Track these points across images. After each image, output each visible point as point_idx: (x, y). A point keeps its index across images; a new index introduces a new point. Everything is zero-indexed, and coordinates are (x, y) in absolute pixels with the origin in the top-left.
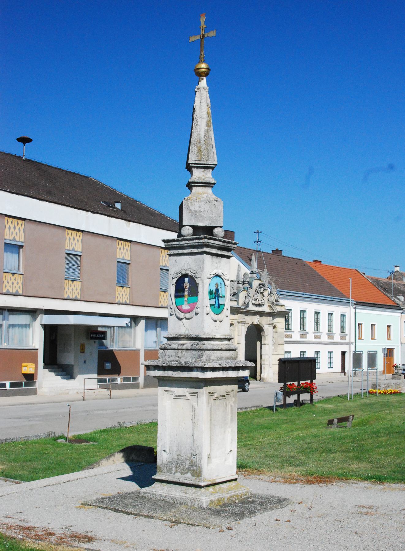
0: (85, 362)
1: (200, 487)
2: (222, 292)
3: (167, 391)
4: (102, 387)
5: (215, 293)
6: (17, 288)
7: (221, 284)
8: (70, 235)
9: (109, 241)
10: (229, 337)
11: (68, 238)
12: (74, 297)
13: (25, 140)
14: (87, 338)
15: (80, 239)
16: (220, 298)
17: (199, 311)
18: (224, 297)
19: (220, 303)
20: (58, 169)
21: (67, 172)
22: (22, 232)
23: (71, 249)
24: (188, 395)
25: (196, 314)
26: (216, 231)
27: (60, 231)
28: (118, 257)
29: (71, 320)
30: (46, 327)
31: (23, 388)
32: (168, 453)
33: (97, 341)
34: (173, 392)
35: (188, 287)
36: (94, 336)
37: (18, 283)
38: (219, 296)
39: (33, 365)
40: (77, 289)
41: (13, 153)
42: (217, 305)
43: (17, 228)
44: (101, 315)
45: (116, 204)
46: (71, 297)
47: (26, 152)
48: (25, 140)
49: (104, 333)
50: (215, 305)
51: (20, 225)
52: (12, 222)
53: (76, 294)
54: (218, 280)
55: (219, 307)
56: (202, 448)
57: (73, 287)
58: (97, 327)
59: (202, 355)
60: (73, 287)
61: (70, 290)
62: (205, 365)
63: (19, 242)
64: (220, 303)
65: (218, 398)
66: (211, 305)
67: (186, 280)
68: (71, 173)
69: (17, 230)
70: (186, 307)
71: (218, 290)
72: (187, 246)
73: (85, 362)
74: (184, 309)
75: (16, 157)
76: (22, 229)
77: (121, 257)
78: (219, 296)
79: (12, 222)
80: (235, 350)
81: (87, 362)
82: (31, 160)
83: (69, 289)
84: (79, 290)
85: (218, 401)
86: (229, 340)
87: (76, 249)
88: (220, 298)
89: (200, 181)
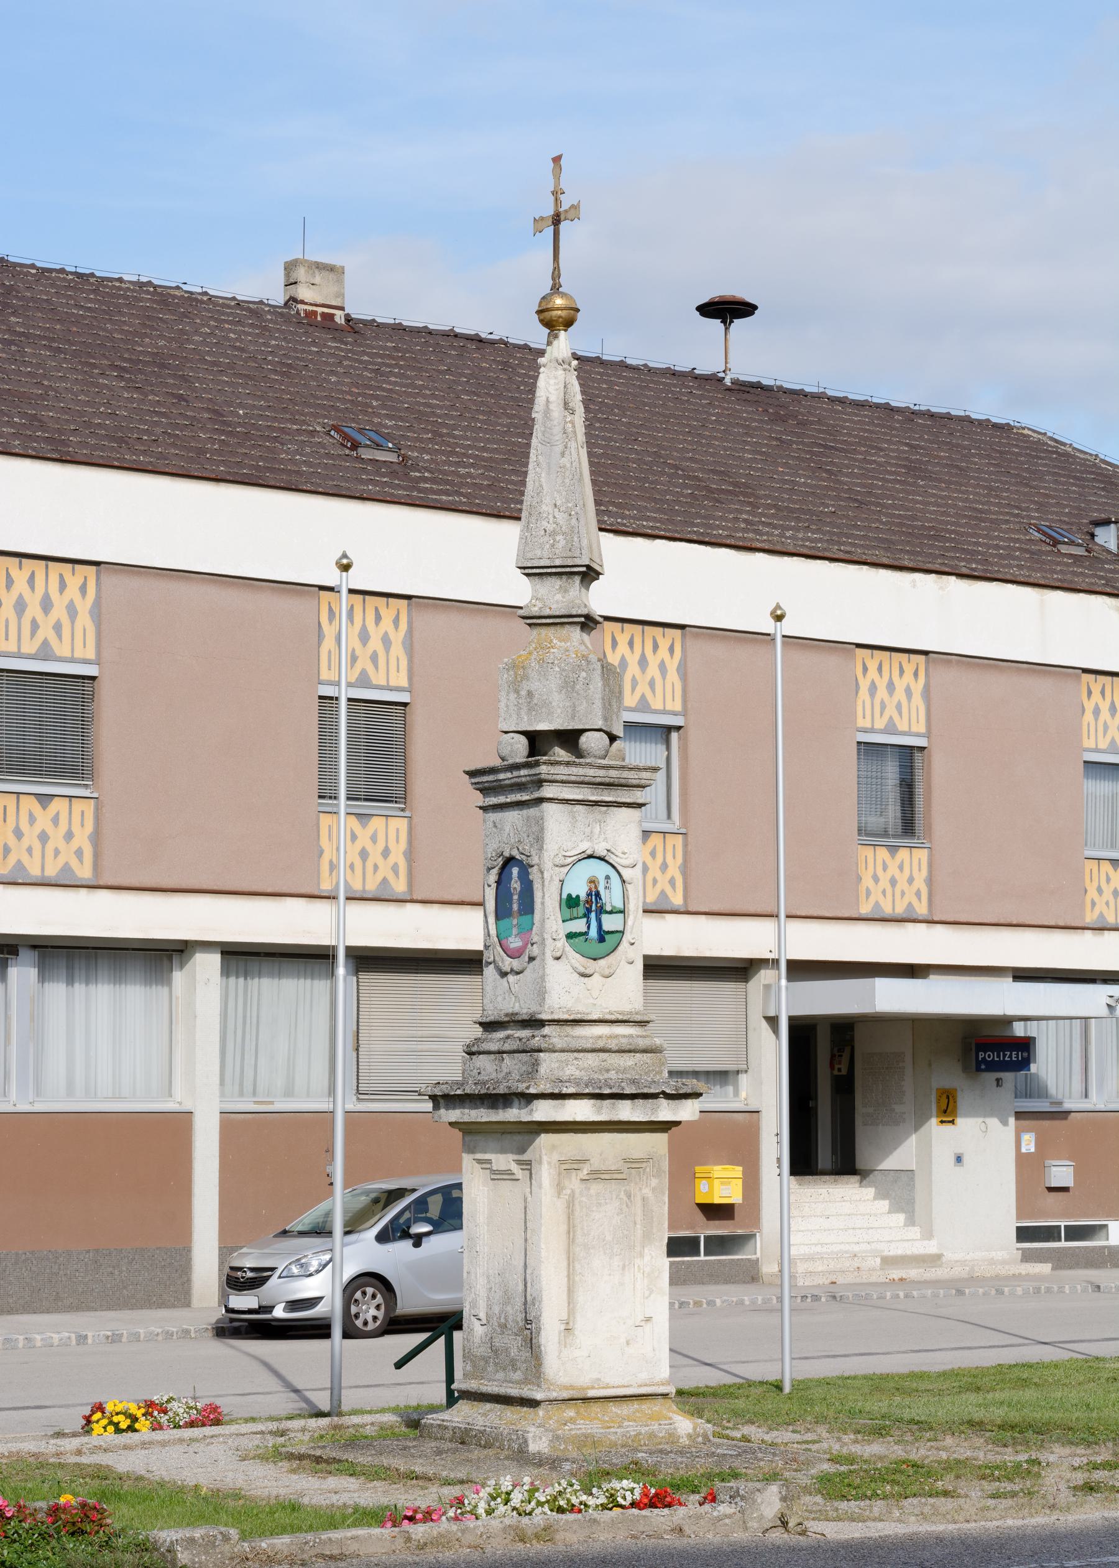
0: (959, 1159)
1: (533, 1403)
2: (612, 897)
3: (479, 1161)
4: (1028, 1257)
5: (588, 902)
6: (663, 884)
7: (608, 877)
8: (872, 672)
9: (1043, 686)
10: (638, 1018)
11: (864, 685)
12: (900, 910)
13: (726, 310)
14: (966, 1069)
15: (918, 687)
16: (604, 917)
17: (535, 950)
18: (622, 912)
19: (606, 927)
20: (878, 406)
21: (910, 415)
22: (673, 676)
23: (880, 724)
24: (515, 1168)
25: (532, 959)
26: (585, 740)
27: (832, 661)
28: (1089, 743)
29: (891, 997)
30: (803, 1035)
31: (702, 1258)
32: (484, 1322)
33: (1008, 1077)
34: (489, 1162)
35: (519, 889)
36: (991, 1056)
37: (664, 867)
38: (601, 910)
39: (738, 1171)
40: (911, 880)
41: (683, 366)
42: (593, 933)
43: (653, 661)
44: (1023, 975)
45: (1099, 531)
46: (888, 910)
47: (747, 354)
48: (726, 310)
49: (1026, 1045)
50: (586, 933)
51: (663, 652)
52: (631, 644)
53: (910, 897)
54: (599, 870)
55: (601, 939)
56: (540, 1302)
57: (893, 870)
58: (1007, 1021)
59: (536, 1064)
60: (893, 870)
61: (884, 883)
62: (528, 1088)
63: (664, 712)
64: (606, 927)
65: (596, 1175)
66: (570, 936)
67: (515, 871)
68: (932, 415)
69: (653, 670)
70: (515, 943)
71: (598, 894)
72: (512, 785)
73: (959, 1159)
74: (512, 946)
75: (697, 377)
76: (672, 665)
77: (1103, 745)
78: (601, 910)
79: (631, 644)
80: (661, 1052)
81: (965, 1159)
82: (758, 386)
83: (876, 879)
84: (920, 883)
85: (595, 1188)
86: (642, 1023)
87: (902, 726)
88: (604, 917)
89: (547, 612)
